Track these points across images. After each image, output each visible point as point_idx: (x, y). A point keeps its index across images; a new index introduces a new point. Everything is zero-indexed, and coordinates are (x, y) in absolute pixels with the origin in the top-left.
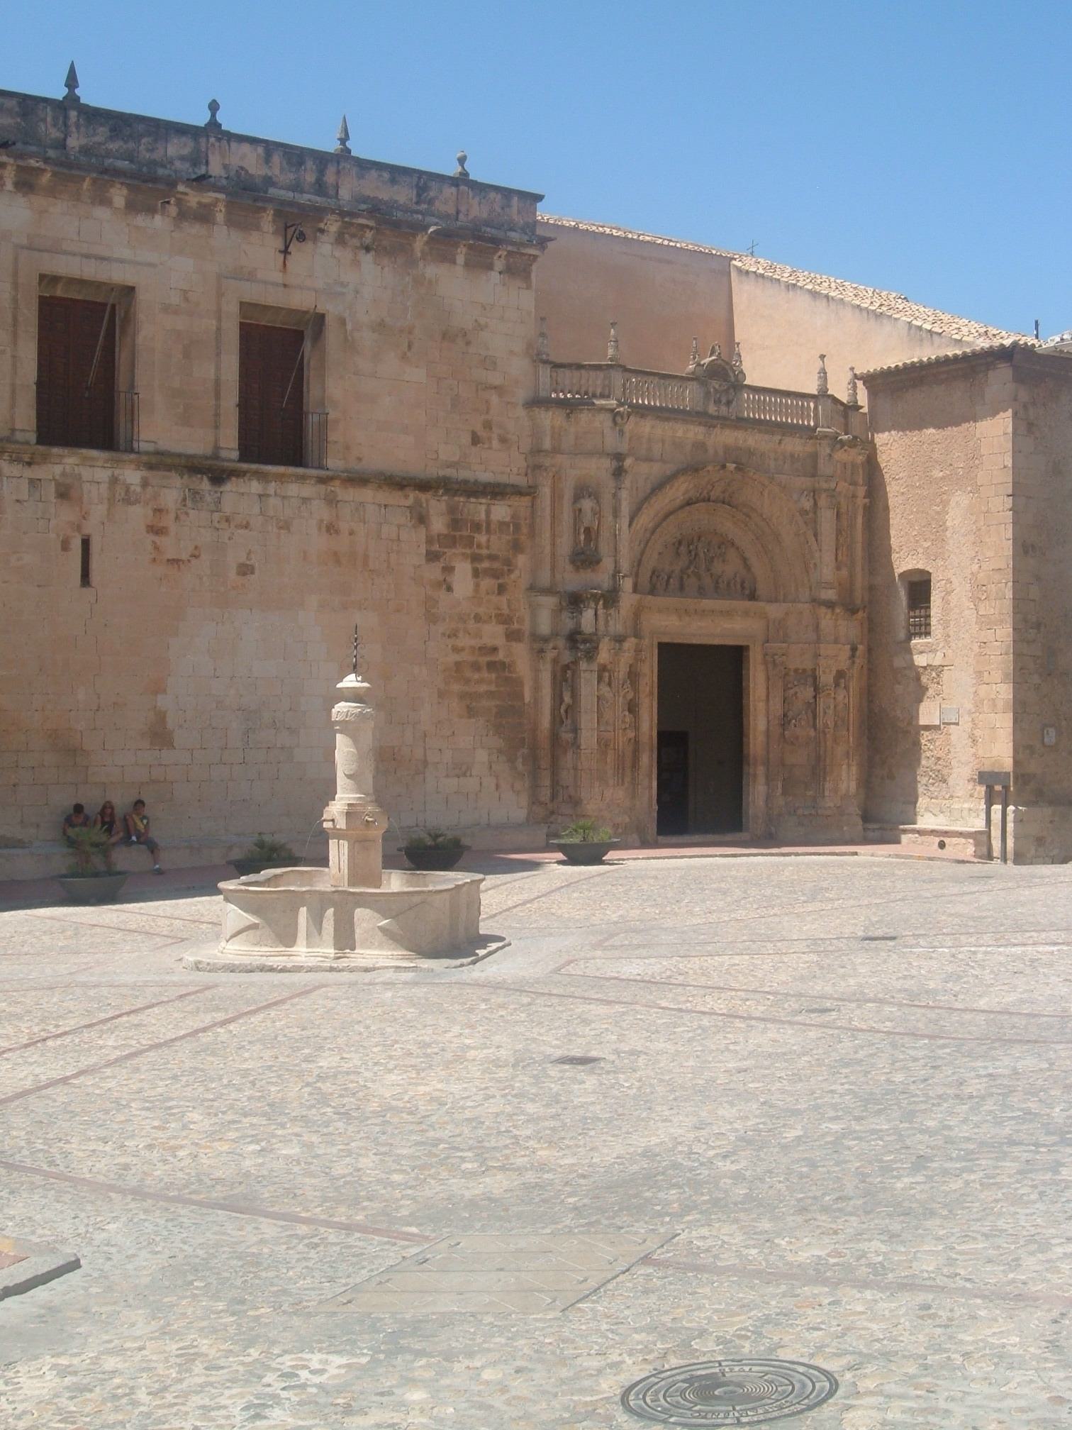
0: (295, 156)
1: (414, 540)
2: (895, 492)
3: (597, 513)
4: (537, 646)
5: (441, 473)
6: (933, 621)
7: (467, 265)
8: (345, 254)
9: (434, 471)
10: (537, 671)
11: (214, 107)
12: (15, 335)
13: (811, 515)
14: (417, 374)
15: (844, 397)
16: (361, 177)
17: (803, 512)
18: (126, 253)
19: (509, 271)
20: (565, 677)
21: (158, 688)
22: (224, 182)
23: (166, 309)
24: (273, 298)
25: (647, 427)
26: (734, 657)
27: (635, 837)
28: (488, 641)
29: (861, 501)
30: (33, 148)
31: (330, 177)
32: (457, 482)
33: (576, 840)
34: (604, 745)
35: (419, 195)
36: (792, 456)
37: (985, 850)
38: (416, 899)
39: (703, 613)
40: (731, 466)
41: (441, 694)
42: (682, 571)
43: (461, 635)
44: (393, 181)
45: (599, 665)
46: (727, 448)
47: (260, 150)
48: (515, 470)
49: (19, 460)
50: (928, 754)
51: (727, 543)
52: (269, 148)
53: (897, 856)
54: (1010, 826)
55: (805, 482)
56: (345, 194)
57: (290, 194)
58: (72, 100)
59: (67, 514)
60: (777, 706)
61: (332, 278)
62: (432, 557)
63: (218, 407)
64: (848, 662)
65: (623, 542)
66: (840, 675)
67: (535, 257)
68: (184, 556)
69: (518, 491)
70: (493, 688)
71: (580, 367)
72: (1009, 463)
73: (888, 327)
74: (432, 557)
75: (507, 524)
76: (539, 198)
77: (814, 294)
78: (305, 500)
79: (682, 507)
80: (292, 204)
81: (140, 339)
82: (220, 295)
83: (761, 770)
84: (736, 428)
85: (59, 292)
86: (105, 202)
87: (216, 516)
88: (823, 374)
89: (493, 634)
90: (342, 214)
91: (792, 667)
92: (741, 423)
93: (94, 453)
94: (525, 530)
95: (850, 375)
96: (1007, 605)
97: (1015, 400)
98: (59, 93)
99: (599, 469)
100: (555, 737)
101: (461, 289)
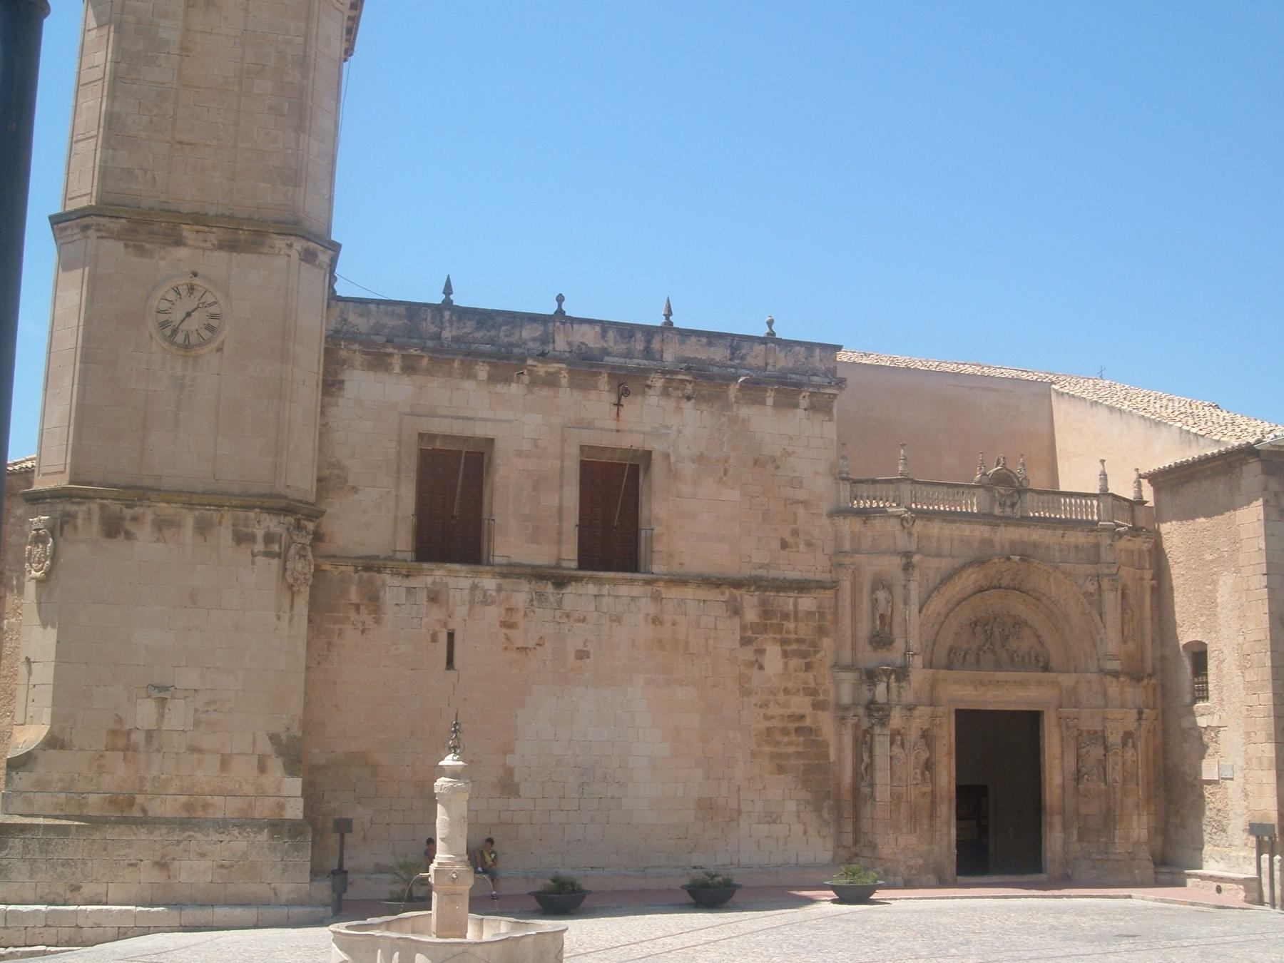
0: (627, 331)
1: (729, 631)
2: (1178, 574)
3: (891, 602)
4: (840, 714)
5: (754, 573)
6: (1211, 687)
7: (775, 405)
8: (670, 404)
9: (747, 572)
10: (839, 734)
11: (560, 299)
12: (398, 479)
13: (1096, 597)
14: (731, 494)
15: (1130, 495)
16: (682, 342)
17: (1087, 594)
18: (488, 414)
19: (813, 408)
20: (864, 742)
21: (508, 749)
22: (568, 355)
23: (520, 454)
24: (607, 441)
25: (935, 528)
26: (1032, 720)
27: (931, 878)
28: (795, 710)
29: (1148, 583)
30: (416, 341)
31: (656, 345)
32: (767, 580)
33: (843, 882)
34: (897, 799)
35: (732, 353)
36: (1076, 547)
37: (1256, 895)
38: (456, 949)
39: (998, 684)
40: (1017, 558)
41: (753, 755)
42: (979, 648)
43: (771, 705)
44: (710, 344)
45: (892, 730)
46: (1013, 544)
47: (598, 328)
48: (820, 568)
49: (398, 574)
50: (1211, 806)
51: (1019, 623)
52: (605, 326)
53: (1163, 901)
54: (1277, 874)
55: (1090, 569)
56: (668, 357)
57: (622, 360)
58: (448, 303)
59: (436, 613)
60: (1071, 765)
61: (660, 424)
62: (745, 641)
63: (561, 527)
64: (1135, 725)
65: (913, 627)
66: (1128, 735)
67: (835, 395)
68: (531, 645)
69: (821, 585)
70: (801, 749)
71: (875, 482)
72: (1263, 546)
73: (1164, 432)
74: (745, 641)
75: (812, 613)
76: (839, 348)
77: (1111, 408)
78: (633, 599)
79: (974, 594)
80: (620, 368)
81: (497, 479)
82: (563, 441)
83: (1057, 820)
84: (1018, 525)
85: (438, 445)
86: (472, 376)
87: (558, 613)
88: (1104, 476)
89: (800, 704)
90: (664, 372)
91: (1084, 728)
92: (1024, 521)
93: (457, 567)
94: (829, 617)
95: (1134, 476)
96: (1267, 672)
97: (1265, 490)
98: (438, 299)
99: (892, 565)
100: (856, 790)
101: (767, 424)
